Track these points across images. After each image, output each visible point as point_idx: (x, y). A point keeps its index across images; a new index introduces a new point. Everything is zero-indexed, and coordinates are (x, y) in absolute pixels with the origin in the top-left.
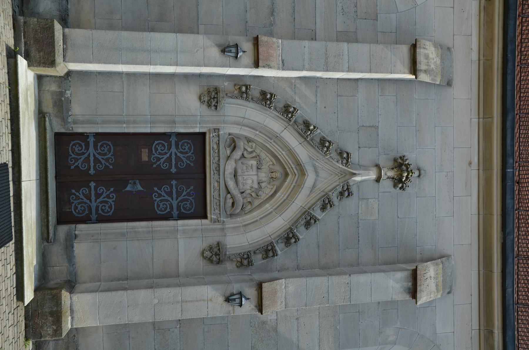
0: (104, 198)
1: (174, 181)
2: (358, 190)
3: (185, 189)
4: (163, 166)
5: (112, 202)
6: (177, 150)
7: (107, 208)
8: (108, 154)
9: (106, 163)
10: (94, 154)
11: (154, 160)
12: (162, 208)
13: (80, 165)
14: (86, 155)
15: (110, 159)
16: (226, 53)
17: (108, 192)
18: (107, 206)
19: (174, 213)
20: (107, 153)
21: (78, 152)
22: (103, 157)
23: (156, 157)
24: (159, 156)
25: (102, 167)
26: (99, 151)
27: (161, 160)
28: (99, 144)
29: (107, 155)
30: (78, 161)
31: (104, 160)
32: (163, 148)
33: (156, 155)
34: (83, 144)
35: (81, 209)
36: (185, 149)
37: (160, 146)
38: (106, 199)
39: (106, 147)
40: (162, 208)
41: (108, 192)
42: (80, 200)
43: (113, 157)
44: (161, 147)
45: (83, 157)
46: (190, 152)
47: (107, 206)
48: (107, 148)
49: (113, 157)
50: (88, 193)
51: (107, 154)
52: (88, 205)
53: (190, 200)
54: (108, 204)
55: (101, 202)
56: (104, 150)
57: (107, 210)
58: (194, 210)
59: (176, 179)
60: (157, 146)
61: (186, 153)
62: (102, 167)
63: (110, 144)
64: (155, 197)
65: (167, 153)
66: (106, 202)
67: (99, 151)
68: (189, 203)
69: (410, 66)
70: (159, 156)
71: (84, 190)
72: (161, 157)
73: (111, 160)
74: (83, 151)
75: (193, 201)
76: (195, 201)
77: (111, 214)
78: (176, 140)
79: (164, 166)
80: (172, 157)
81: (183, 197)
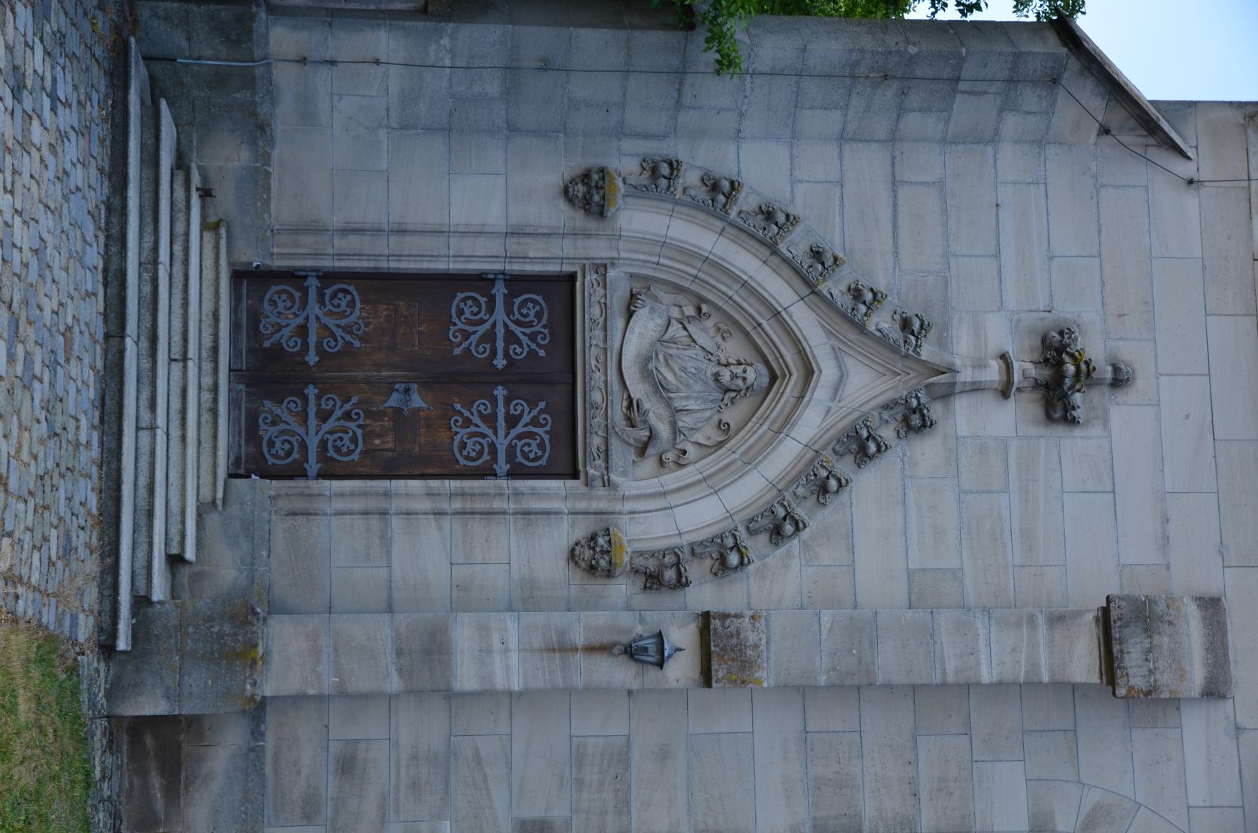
0: (526, 425)
1: (500, 388)
3: (339, 404)
4: (477, 352)
5: (544, 435)
6: (509, 318)
7: (534, 447)
9: (531, 344)
12: (471, 451)
13: (473, 349)
14: (487, 326)
15: (540, 336)
17: (535, 412)
18: (534, 444)
19: (311, 467)
20: (534, 321)
21: (470, 317)
22: (338, 322)
23: (461, 330)
25: (522, 353)
26: (517, 316)
28: (518, 301)
29: (533, 326)
31: (340, 330)
32: (291, 304)
33: (461, 326)
34: (483, 300)
35: (475, 448)
37: (282, 299)
38: (530, 429)
40: (471, 451)
41: (535, 412)
42: (472, 427)
43: (546, 331)
44: (285, 301)
46: (538, 323)
47: (534, 444)
49: (546, 331)
50: (300, 409)
51: (347, 314)
52: (300, 440)
53: (540, 436)
54: (536, 439)
55: (520, 437)
56: (339, 305)
57: (348, 447)
58: (547, 461)
59: (504, 383)
61: (529, 325)
62: (522, 353)
64: (455, 424)
65: (486, 321)
66: (531, 435)
67: (517, 316)
68: (538, 445)
71: (481, 406)
72: (470, 329)
74: (482, 315)
75: (546, 438)
76: (550, 440)
77: (543, 462)
79: (480, 351)
80: (496, 330)
81: (523, 427)
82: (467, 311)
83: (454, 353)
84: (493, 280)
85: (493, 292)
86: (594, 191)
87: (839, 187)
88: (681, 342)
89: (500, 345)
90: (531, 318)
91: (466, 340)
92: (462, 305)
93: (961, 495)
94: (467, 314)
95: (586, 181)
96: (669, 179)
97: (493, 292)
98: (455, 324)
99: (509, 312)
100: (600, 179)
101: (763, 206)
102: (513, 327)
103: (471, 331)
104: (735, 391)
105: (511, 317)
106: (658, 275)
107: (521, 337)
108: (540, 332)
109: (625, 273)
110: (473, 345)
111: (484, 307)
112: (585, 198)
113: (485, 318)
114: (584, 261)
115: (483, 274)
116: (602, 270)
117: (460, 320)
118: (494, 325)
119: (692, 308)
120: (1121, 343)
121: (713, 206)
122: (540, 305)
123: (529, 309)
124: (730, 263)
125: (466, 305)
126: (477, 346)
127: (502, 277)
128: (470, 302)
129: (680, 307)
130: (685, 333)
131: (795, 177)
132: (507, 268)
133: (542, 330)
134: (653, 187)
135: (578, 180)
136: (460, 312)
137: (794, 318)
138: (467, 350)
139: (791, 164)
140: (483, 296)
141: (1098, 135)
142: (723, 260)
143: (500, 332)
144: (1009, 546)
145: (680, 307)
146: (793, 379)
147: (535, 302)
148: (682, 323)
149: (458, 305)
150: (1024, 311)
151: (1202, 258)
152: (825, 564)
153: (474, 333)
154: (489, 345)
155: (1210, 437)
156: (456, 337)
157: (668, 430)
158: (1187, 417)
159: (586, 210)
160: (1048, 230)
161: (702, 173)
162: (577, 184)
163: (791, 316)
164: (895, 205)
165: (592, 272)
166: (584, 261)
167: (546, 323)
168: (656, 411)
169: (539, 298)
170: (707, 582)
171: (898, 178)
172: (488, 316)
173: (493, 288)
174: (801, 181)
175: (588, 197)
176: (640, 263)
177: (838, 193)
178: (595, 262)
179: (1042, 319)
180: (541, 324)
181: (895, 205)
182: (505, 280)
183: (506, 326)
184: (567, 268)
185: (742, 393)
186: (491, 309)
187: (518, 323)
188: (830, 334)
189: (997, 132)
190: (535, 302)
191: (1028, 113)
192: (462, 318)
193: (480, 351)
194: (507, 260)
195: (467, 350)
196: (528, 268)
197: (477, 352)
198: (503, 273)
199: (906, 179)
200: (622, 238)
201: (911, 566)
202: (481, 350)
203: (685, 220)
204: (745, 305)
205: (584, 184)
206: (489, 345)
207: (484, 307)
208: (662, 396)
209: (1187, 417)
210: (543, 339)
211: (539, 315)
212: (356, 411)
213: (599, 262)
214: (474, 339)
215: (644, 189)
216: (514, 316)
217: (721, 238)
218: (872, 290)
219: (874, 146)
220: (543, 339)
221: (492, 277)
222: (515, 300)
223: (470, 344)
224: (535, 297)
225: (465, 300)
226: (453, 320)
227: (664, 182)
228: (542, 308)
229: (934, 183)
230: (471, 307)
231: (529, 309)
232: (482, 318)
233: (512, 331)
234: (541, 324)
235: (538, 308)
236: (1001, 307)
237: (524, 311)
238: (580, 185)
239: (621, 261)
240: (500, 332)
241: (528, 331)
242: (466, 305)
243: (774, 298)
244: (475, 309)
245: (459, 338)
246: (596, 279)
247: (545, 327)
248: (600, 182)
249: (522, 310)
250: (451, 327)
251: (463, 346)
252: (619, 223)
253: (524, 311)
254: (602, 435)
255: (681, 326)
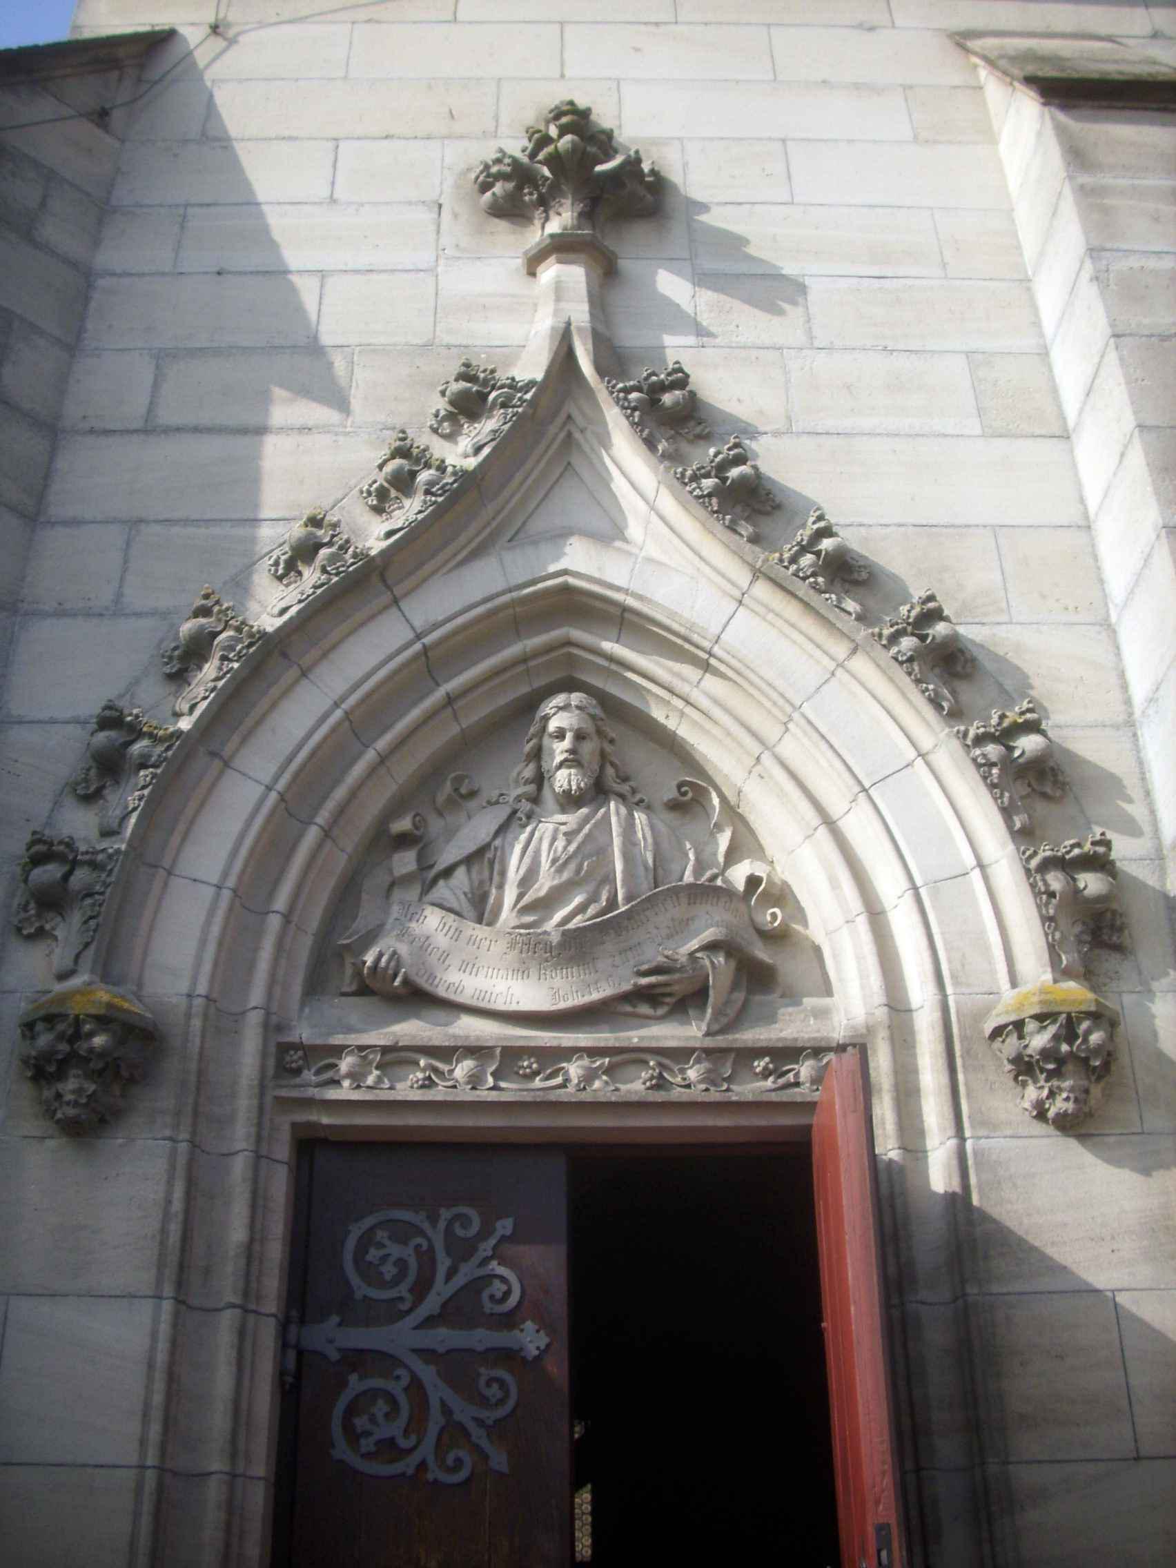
2: (419, 135)
4: (501, 1402)
8: (429, 1240)
10: (416, 1328)
11: (459, 1462)
13: (491, 1416)
14: (427, 1373)
15: (460, 1232)
16: (1112, 340)
24: (433, 1429)
26: (403, 1290)
27: (458, 1416)
28: (362, 1289)
29: (431, 1249)
30: (462, 1428)
36: (402, 1264)
39: (382, 1252)
43: (445, 1214)
45: (438, 1390)
46: (422, 1233)
48: (387, 1242)
49: (445, 1214)
60: (367, 1445)
61: (427, 1259)
63: (369, 1222)
67: (403, 1290)
69: (1093, 107)
70: (433, 1429)
72: (436, 1420)
73: (464, 1227)
74: (397, 1388)
78: (335, 1319)
79: (499, 1394)
80: (441, 1350)
82: (386, 1430)
83: (505, 1469)
84: (300, 1353)
85: (334, 1356)
86: (82, 1047)
87: (143, 527)
88: (481, 883)
89: (481, 1338)
90: (408, 1253)
91: (467, 1435)
92: (367, 1445)
93: (817, 344)
94: (394, 1429)
95: (52, 1068)
96: (75, 864)
97: (334, 1356)
98: (422, 1466)
99: (391, 1311)
100: (51, 1029)
101: (167, 670)
102: (432, 1304)
103: (442, 1421)
104: (602, 768)
105: (404, 1307)
106: (314, 922)
107: (460, 1280)
108: (449, 1231)
109: (303, 1005)
110: (484, 1414)
111: (378, 1383)
112: (100, 1073)
113: (405, 1381)
114: (268, 1099)
115: (282, 1384)
116: (294, 1057)
117: (410, 1451)
118: (427, 1354)
119: (397, 857)
120: (504, 119)
121: (155, 766)
122: (372, 1229)
123: (384, 1258)
124: (300, 747)
125: (368, 1434)
126: (484, 1402)
127: (293, 1329)
128: (360, 1422)
129: (392, 885)
130: (461, 872)
131: (107, 608)
132: (273, 1310)
133: (442, 1225)
134: (89, 901)
135: (48, 1094)
136: (388, 1449)
137: (440, 618)
138: (497, 1430)
139: (75, 615)
140: (344, 1384)
141: (107, 132)
142: (290, 760)
143: (445, 1337)
144: (909, 282)
145: (392, 885)
146: (577, 634)
147: (366, 1242)
148: (434, 881)
149: (367, 1456)
150: (438, 240)
151: (353, 23)
152: (999, 577)
153: (447, 1411)
154: (482, 1370)
155: (673, 27)
156: (459, 1462)
157: (709, 907)
158: (637, 50)
159: (132, 1080)
160: (279, 203)
161: (69, 802)
162: (59, 1096)
163: (436, 626)
164: (196, 430)
165: (298, 1081)
166: (268, 1099)
167: (423, 1215)
168: (665, 932)
169: (356, 1231)
170: (1082, 811)
171: (138, 424)
172: (400, 1371)
173: (324, 1356)
174: (119, 595)
175: (97, 1065)
176: (283, 962)
177: (157, 528)
178: (271, 1071)
179: (456, 216)
180: (426, 1226)
181: (196, 430)
182: (302, 1321)
183: (429, 1322)
184: (283, 1150)
185: (609, 748)
186: (384, 1361)
187: (422, 1288)
188: (477, 553)
189: (74, 265)
190: (366, 1242)
191: (43, 204)
192: (404, 1443)
193: (499, 1394)
194: (252, 1307)
195: (497, 1430)
196: (275, 1251)
197: (501, 1402)
198: (284, 1327)
199: (143, 410)
200: (214, 995)
201: (978, 431)
202: (494, 1392)
203: (184, 839)
204: (401, 726)
205: (60, 1075)
206: (482, 1370)
207: (378, 1383)
208: (628, 915)
209: (637, 50)
210: (465, 1221)
211: (402, 1232)
212: (690, 795)
213: (271, 1062)
214: (464, 1412)
215: (92, 923)
216: (401, 1299)
217: (237, 763)
218: (381, 430)
219: (61, 464)
220: (465, 1221)
221: (292, 1355)
222: (358, 1295)
223: (480, 1422)
224: (351, 1244)
225: (353, 1436)
226: (410, 1471)
227: (81, 876)
228: (380, 1225)
229: (157, 367)
230: (373, 1420)
231: (384, 1258)
232: (406, 1389)
233: (444, 1305)
234: (426, 1226)
235: (381, 1235)
236: (432, 271)
237: (389, 1271)
238: (60, 1086)
239: (274, 1008)
240: (445, 1337)
241: (443, 1264)
242: (368, 1434)
243: (391, 658)
244: (381, 1407)
245: (461, 1453)
246: (318, 1073)
247: (433, 1219)
248: (61, 1027)
249: (388, 1277)
250: (430, 1477)
251: (484, 1443)
252: (174, 1000)
253: (389, 1271)
254: (729, 1064)
255: (441, 883)
